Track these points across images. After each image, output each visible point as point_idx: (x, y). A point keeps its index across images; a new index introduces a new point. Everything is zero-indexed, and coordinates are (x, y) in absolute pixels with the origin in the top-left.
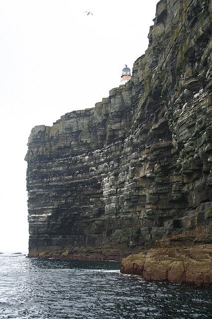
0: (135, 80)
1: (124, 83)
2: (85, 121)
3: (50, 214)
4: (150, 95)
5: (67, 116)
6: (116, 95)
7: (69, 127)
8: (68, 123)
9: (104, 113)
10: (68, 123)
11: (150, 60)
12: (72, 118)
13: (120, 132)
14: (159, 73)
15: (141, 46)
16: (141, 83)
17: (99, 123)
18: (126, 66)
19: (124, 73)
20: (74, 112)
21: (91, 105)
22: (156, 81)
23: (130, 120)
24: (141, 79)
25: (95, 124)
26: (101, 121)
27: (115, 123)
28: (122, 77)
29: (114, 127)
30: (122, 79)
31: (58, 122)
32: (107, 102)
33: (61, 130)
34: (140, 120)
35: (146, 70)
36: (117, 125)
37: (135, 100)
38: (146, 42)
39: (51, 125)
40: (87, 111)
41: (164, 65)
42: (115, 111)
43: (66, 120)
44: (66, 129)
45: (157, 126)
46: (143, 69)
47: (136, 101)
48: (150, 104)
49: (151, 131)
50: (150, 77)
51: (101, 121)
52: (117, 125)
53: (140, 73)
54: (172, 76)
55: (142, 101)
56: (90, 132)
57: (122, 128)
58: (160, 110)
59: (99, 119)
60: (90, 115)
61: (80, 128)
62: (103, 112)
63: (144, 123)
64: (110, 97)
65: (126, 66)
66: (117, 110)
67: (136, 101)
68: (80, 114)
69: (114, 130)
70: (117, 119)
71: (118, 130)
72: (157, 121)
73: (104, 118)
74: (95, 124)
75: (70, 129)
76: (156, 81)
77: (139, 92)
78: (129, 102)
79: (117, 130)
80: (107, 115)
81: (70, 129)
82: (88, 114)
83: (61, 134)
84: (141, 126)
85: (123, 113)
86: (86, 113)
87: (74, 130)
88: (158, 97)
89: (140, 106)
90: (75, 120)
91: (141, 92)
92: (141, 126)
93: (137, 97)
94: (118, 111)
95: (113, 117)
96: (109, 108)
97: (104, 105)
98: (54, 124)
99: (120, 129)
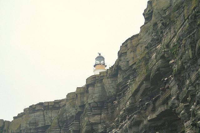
0: (122, 64)
1: (97, 73)
2: (53, 115)
3: (191, 110)
4: (147, 78)
5: (32, 109)
6: (95, 83)
7: (34, 122)
8: (33, 116)
9: (79, 104)
10: (33, 116)
11: (148, 39)
12: (38, 110)
13: (100, 126)
14: (164, 51)
15: (135, 24)
16: (131, 67)
17: (73, 116)
18: (100, 54)
19: (97, 61)
20: (41, 104)
21: (62, 96)
22: (157, 61)
23: (112, 113)
24: (131, 63)
25: (67, 117)
26: (74, 114)
27: (94, 115)
28: (95, 66)
29: (92, 120)
30: (95, 68)
31: (20, 116)
32: (82, 92)
33: (24, 125)
34: (130, 111)
35: (137, 52)
36: (97, 118)
37: (121, 90)
38: (142, 21)
39: (11, 119)
40: (57, 102)
41: (175, 40)
42: (95, 102)
43: (30, 113)
44: (30, 124)
45: (154, 116)
46: (134, 51)
47: (123, 88)
48: (146, 89)
49: (145, 122)
50: (147, 60)
51: (74, 114)
52: (97, 118)
53: (130, 55)
54: (192, 50)
55: (134, 87)
56: (60, 127)
57: (102, 121)
58: (159, 97)
59: (72, 112)
60: (60, 107)
61: (48, 122)
62: (78, 103)
63: (136, 114)
64: (88, 86)
65: (100, 54)
66: (96, 100)
67: (123, 88)
68: (48, 106)
69: (92, 124)
70: (96, 111)
71: (98, 124)
72: (154, 110)
73: (79, 110)
74: (67, 117)
75: (36, 123)
76: (157, 61)
77: (128, 78)
78: (112, 90)
79: (96, 124)
80: (83, 106)
81: (36, 123)
82: (57, 106)
83: (24, 130)
84: (131, 117)
85: (105, 104)
86: (56, 105)
87: (40, 126)
88: (156, 82)
89: (129, 94)
90: (42, 113)
91: (131, 77)
92: (131, 117)
93: (126, 84)
94: (99, 102)
95: (91, 109)
96: (85, 99)
97: (79, 96)
98: (15, 118)
99: (100, 123)
